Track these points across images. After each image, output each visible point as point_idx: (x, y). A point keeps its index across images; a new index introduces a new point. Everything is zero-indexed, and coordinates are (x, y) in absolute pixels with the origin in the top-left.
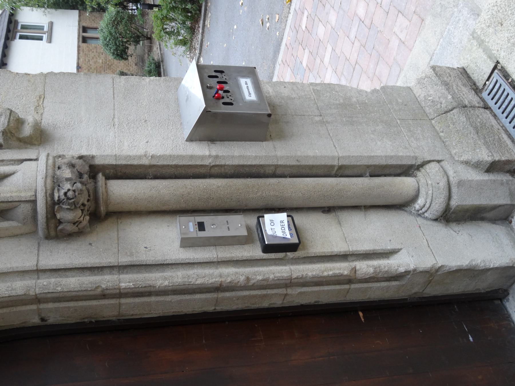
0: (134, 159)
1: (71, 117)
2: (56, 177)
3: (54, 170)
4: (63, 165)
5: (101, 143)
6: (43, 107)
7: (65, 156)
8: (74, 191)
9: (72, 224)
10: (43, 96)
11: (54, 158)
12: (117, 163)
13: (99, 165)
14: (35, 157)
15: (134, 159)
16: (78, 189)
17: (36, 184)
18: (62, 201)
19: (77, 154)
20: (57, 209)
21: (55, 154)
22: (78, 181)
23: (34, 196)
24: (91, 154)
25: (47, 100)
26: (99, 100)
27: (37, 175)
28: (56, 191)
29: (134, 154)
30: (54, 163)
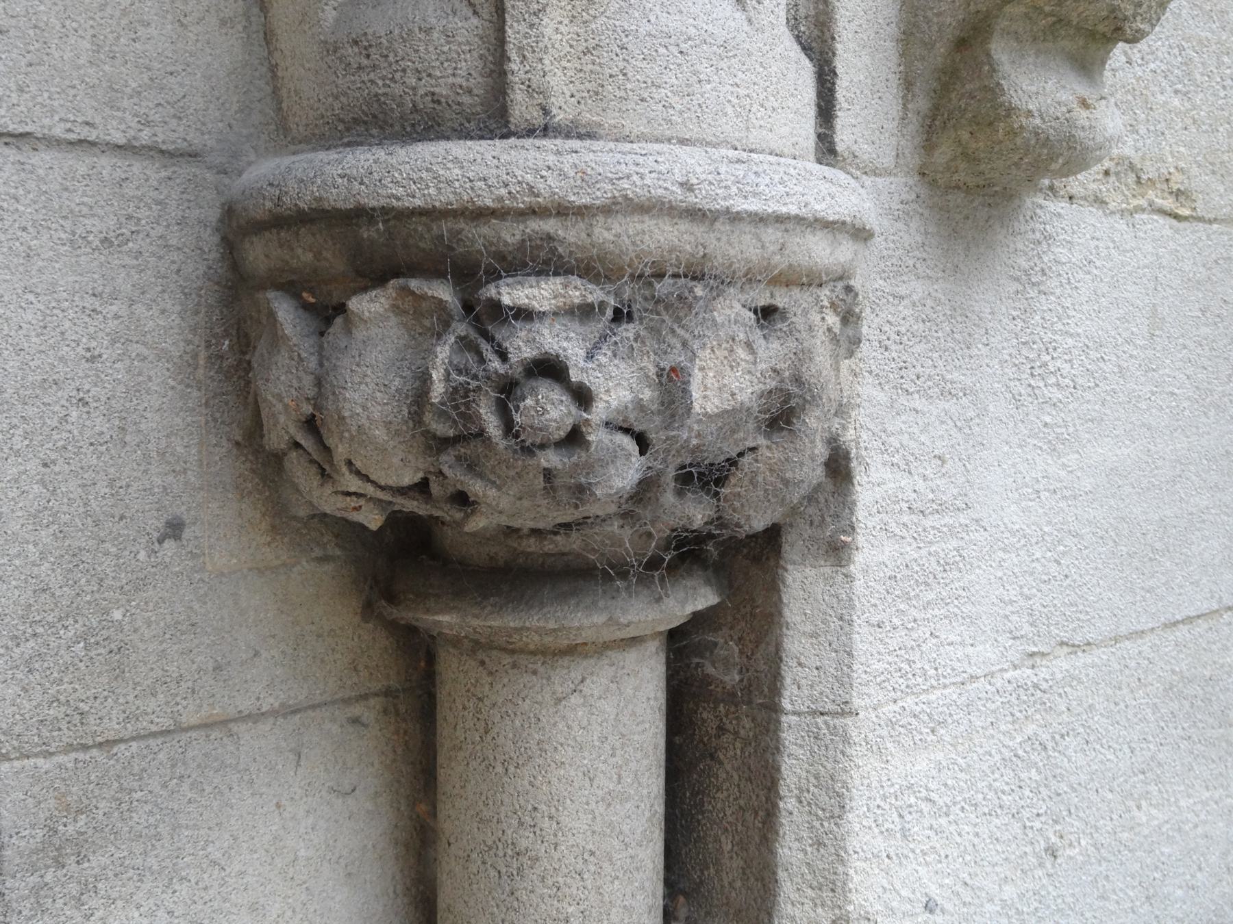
0: (819, 844)
1: (1080, 381)
2: (699, 291)
3: (750, 279)
4: (792, 344)
5: (930, 596)
6: (1140, 209)
7: (851, 354)
8: (574, 438)
9: (307, 409)
10: (1185, 212)
11: (842, 276)
12: (794, 719)
13: (774, 587)
14: (844, 137)
15: (819, 844)
16: (589, 468)
17: (641, 138)
18: (489, 338)
19: (865, 436)
20: (424, 297)
21: (867, 282)
22: (658, 465)
23: (537, 118)
24: (861, 540)
25: (1169, 232)
26: (1161, 539)
27: (715, 146)
28: (578, 291)
29: (853, 843)
30: (808, 279)
